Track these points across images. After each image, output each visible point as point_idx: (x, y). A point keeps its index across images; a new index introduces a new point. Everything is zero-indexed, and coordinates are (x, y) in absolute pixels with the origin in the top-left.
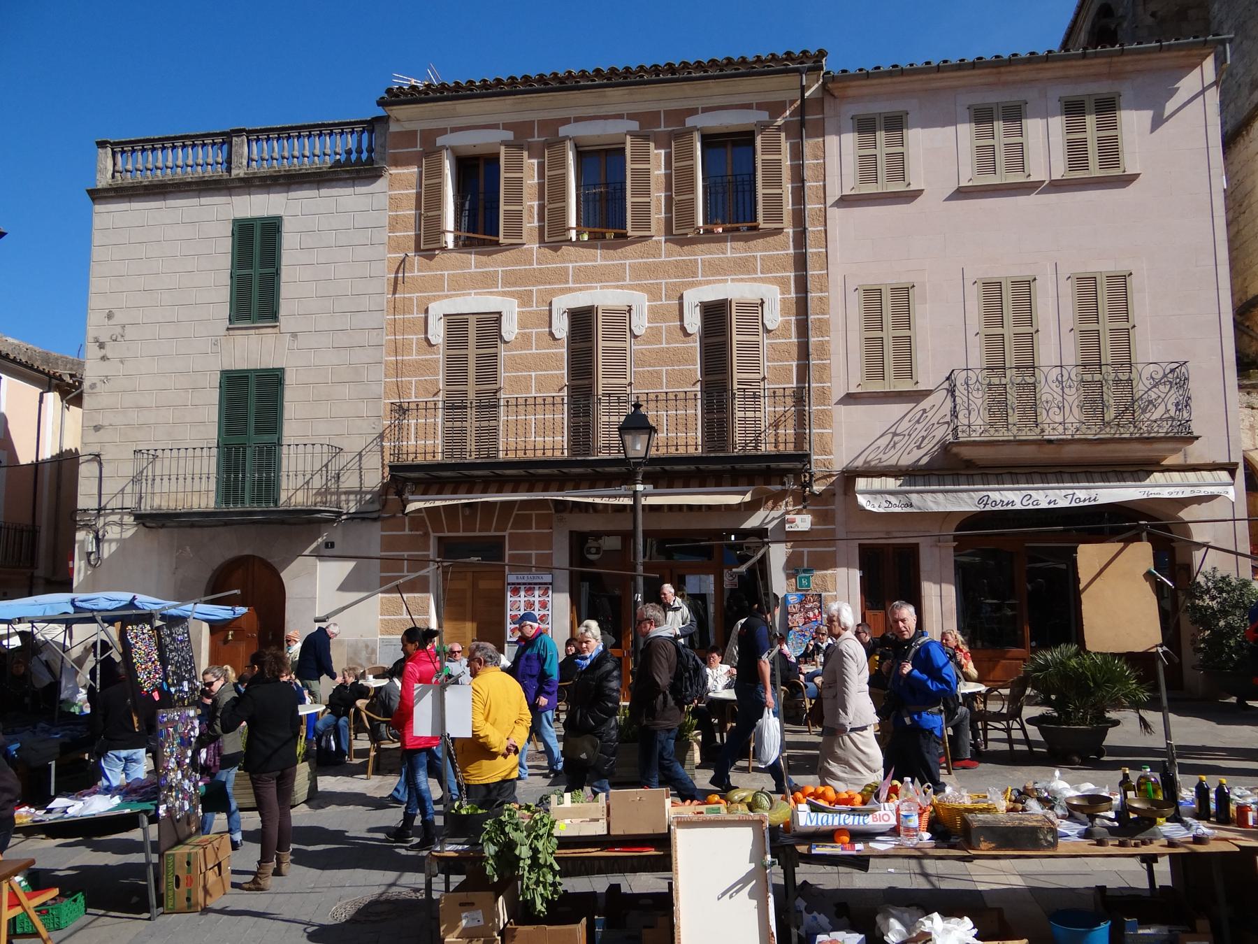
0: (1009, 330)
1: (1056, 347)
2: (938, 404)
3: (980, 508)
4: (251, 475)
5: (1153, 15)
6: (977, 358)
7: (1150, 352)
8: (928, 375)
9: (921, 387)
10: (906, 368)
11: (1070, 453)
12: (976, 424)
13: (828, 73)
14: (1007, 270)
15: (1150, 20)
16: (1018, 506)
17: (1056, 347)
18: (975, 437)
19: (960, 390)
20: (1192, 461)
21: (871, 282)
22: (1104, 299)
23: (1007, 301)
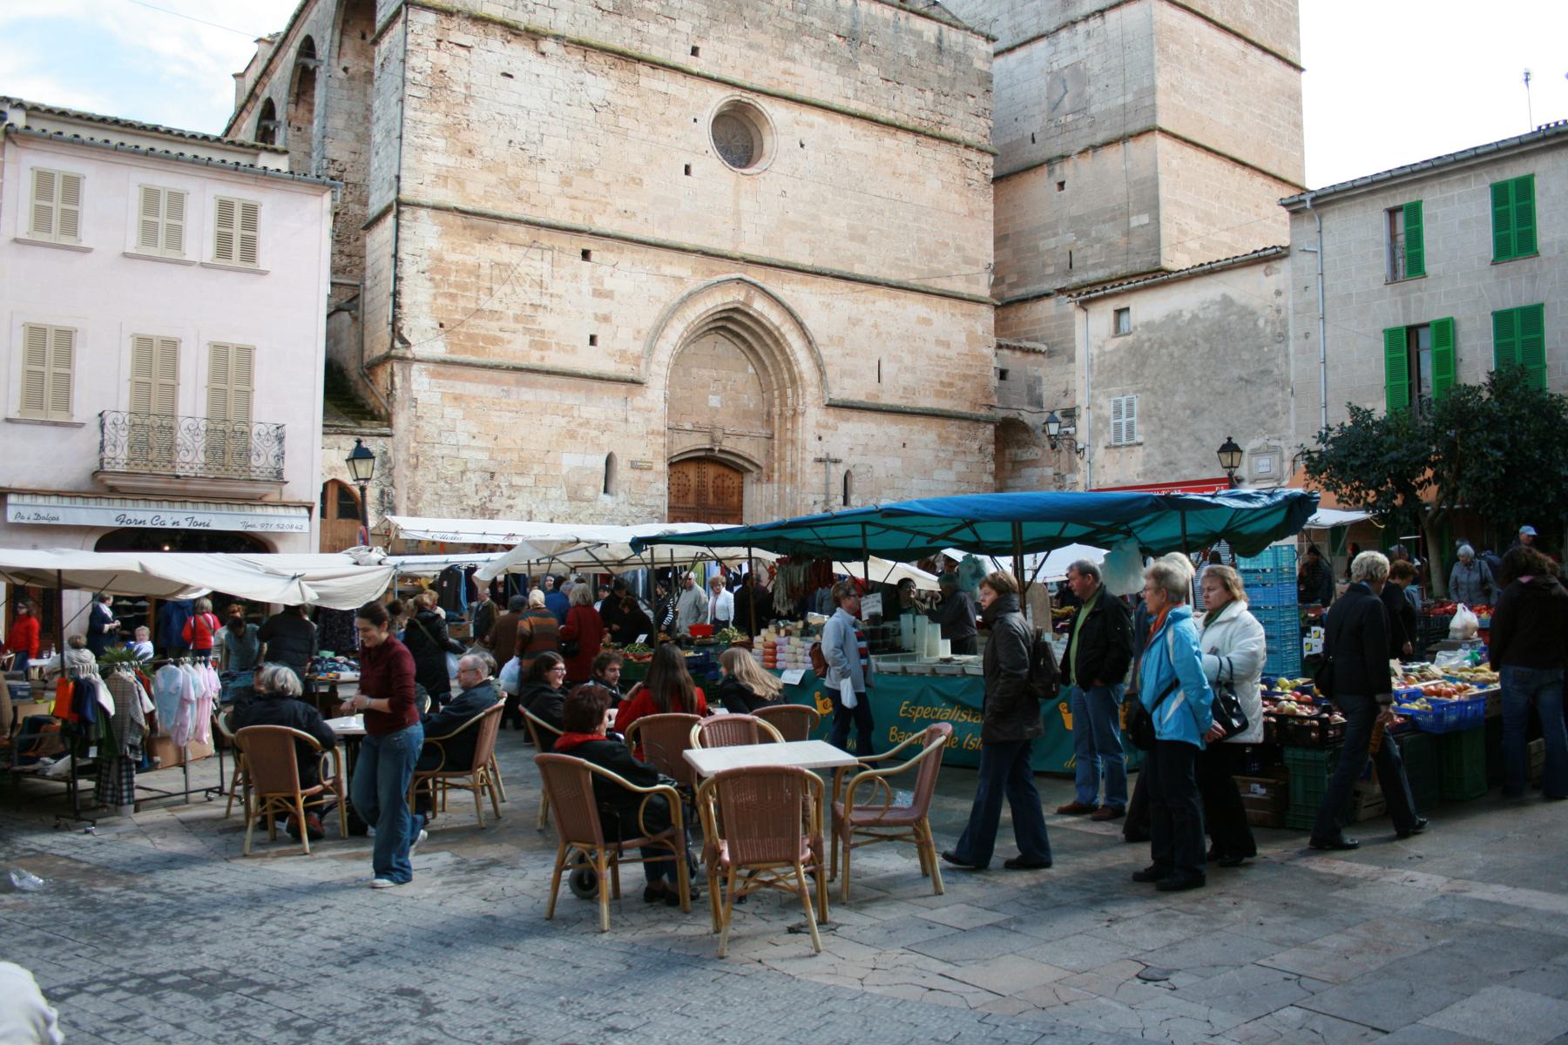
0: (49, 369)
1: (192, 404)
2: (90, 437)
3: (117, 524)
4: (1513, 230)
5: (345, 70)
6: (124, 404)
7: (264, 413)
8: (84, 407)
9: (75, 420)
10: (65, 402)
11: (193, 487)
12: (119, 457)
13: (11, 125)
14: (157, 329)
15: (341, 74)
16: (148, 525)
17: (192, 404)
18: (119, 468)
19: (109, 428)
20: (285, 499)
21: (36, 320)
22: (233, 367)
23: (155, 358)
